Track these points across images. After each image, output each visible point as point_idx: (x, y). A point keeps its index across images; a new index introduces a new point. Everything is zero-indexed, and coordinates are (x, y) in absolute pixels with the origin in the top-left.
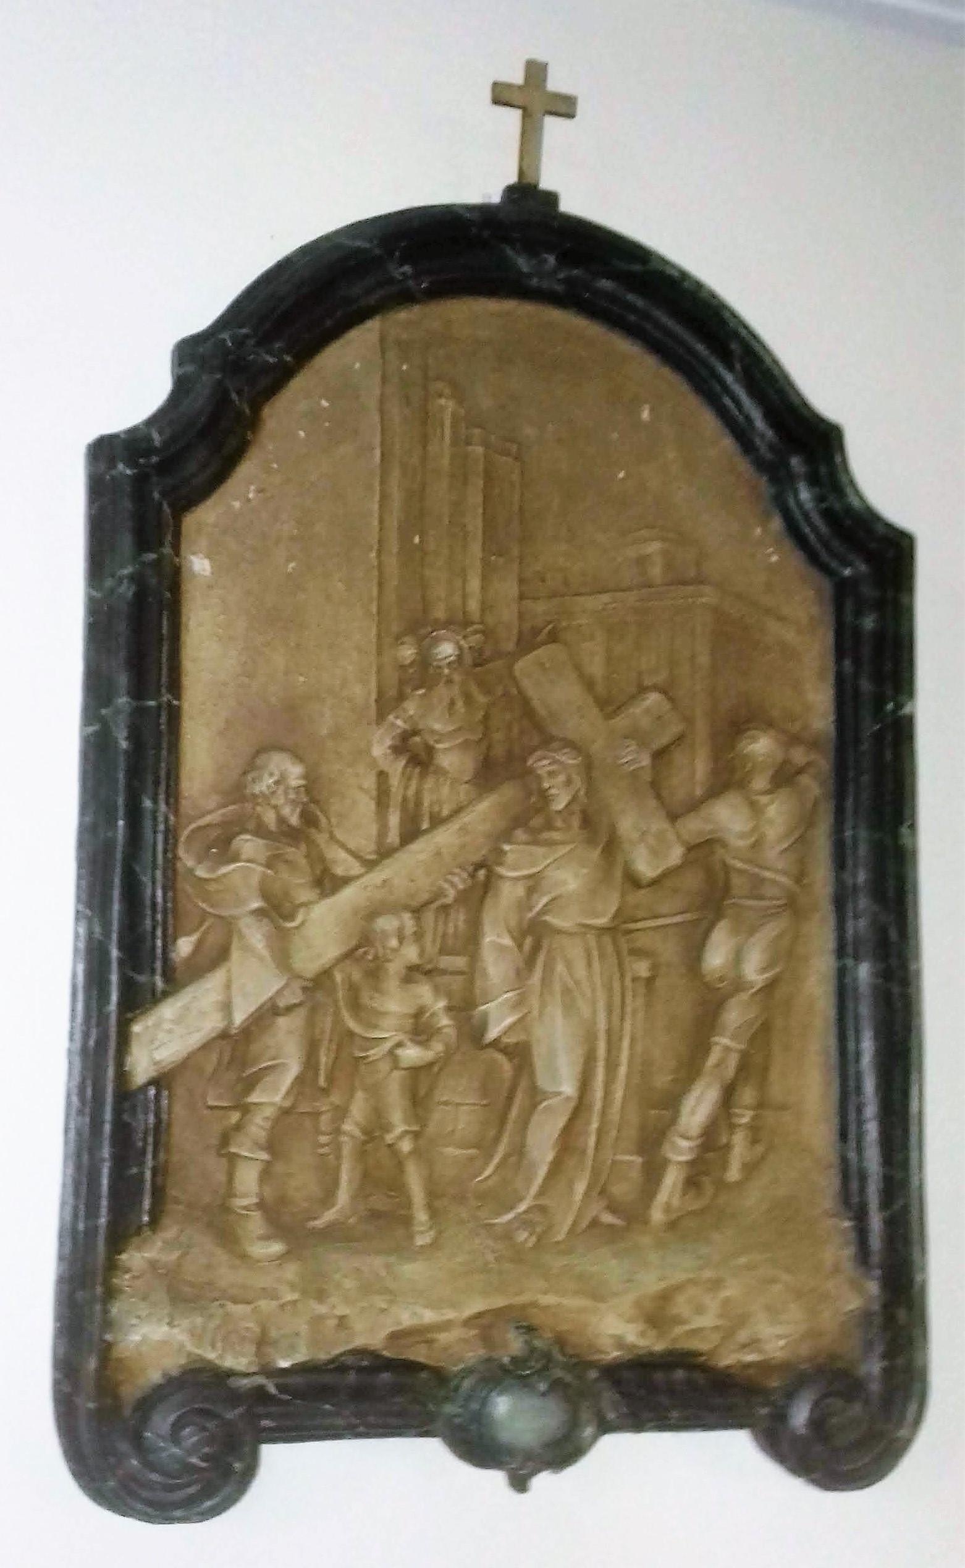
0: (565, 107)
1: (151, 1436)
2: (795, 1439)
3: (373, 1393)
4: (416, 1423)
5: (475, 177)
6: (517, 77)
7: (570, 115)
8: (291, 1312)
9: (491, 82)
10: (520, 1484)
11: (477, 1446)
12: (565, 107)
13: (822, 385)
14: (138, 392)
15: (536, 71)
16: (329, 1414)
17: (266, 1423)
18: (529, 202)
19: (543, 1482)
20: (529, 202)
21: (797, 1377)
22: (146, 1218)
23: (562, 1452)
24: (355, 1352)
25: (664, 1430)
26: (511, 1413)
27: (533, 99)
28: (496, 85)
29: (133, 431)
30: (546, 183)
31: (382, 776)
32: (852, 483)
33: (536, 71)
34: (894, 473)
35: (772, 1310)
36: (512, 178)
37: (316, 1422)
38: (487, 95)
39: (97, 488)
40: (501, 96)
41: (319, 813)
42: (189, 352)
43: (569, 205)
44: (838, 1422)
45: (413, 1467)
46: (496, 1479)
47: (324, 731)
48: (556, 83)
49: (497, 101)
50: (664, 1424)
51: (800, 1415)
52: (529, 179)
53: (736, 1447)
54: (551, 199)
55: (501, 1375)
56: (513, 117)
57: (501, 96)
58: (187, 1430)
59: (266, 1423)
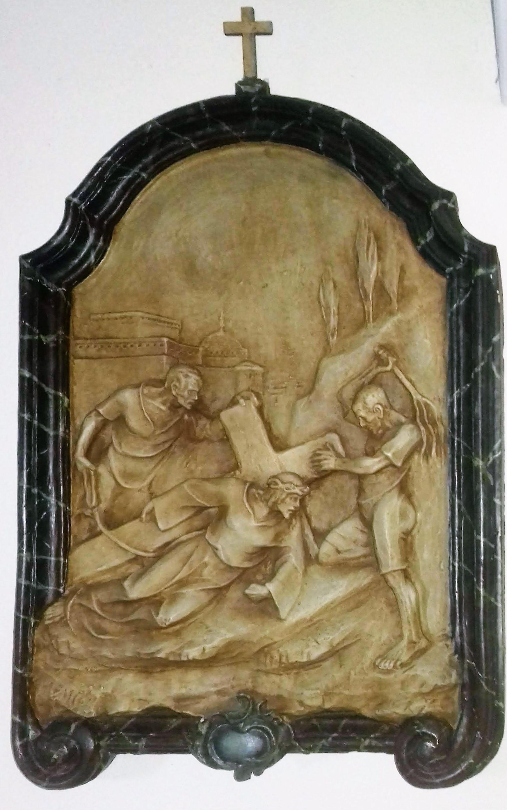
0: (267, 30)
1: (60, 745)
3: (159, 731)
5: (222, 83)
6: (237, 17)
7: (271, 34)
11: (214, 754)
13: (436, 171)
14: (43, 224)
15: (248, 13)
24: (118, 713)
26: (251, 743)
27: (249, 29)
30: (261, 76)
32: (49, 243)
33: (248, 13)
34: (479, 220)
35: (424, 683)
36: (240, 77)
37: (374, 723)
39: (22, 268)
40: (231, 30)
44: (439, 745)
45: (181, 768)
46: (228, 775)
54: (265, 86)
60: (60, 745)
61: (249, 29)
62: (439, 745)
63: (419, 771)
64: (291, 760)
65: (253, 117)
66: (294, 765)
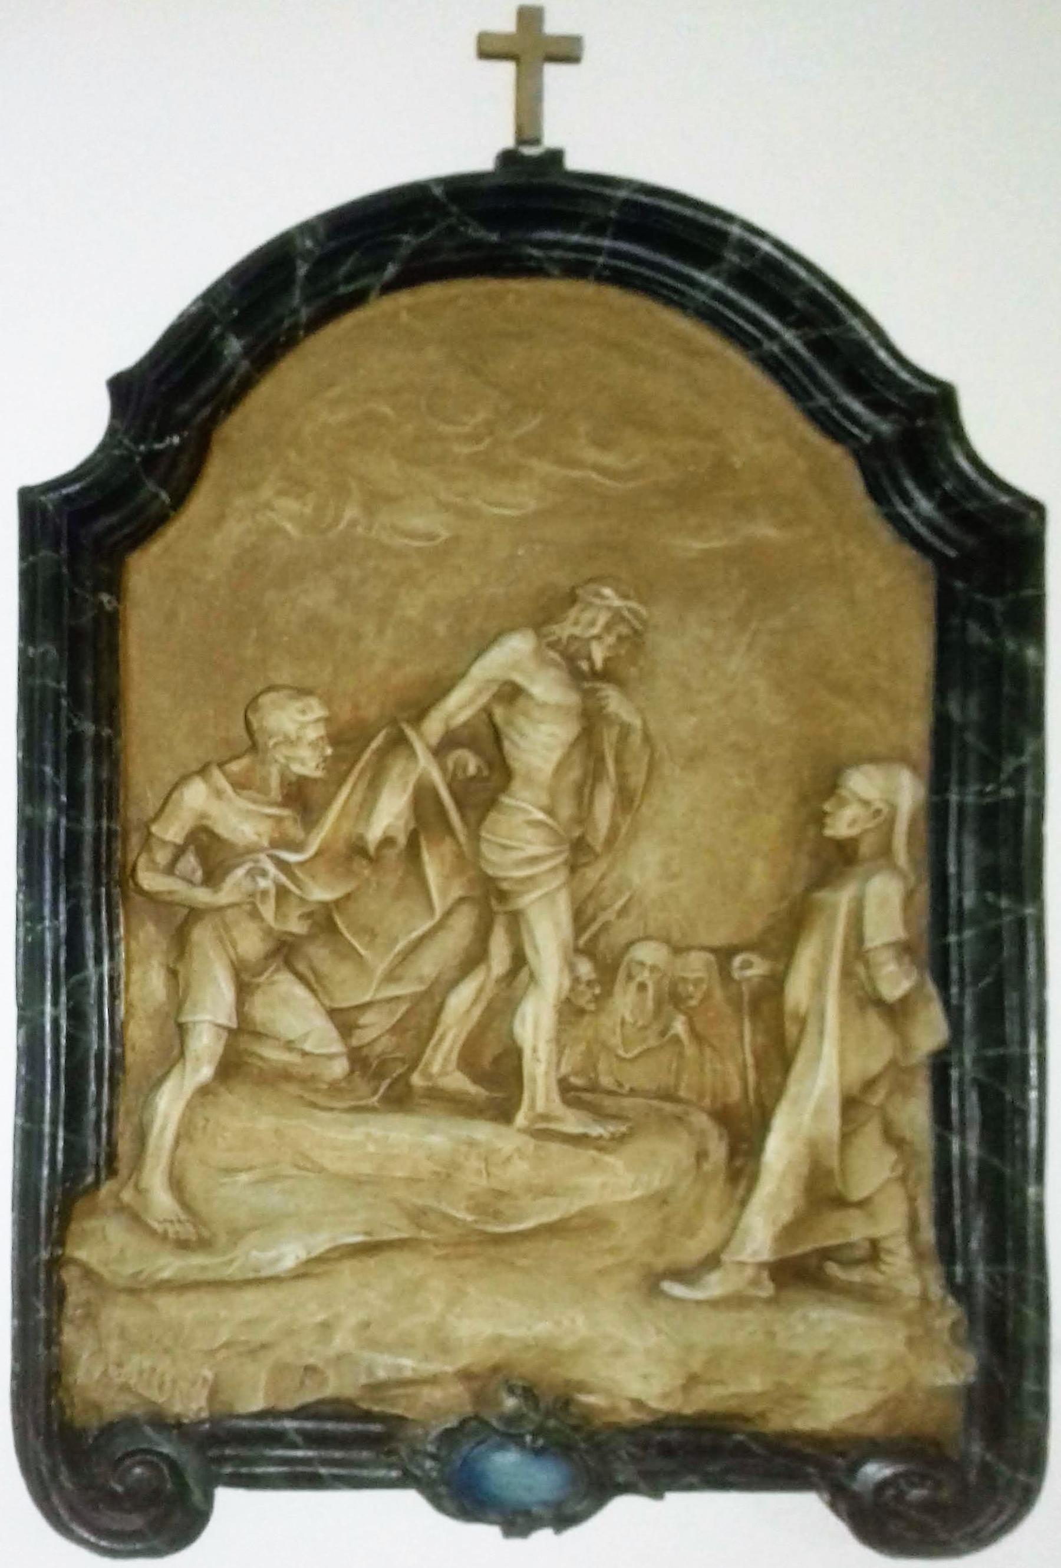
0: (567, 52)
1: (122, 1473)
3: (342, 1441)
5: (465, 139)
9: (476, 31)
11: (465, 1496)
12: (567, 52)
14: (72, 432)
15: (530, 18)
16: (57, 799)
22: (64, 702)
26: (509, 1468)
27: (530, 49)
30: (551, 139)
31: (712, 1261)
33: (530, 18)
36: (507, 140)
38: (472, 49)
40: (490, 49)
41: (122, 919)
42: (123, 388)
43: (574, 163)
47: (434, 1283)
48: (554, 25)
49: (485, 54)
54: (555, 157)
56: (507, 70)
61: (530, 49)
62: (930, 1482)
63: (872, 1520)
64: (626, 1511)
65: (521, 220)
66: (626, 1517)
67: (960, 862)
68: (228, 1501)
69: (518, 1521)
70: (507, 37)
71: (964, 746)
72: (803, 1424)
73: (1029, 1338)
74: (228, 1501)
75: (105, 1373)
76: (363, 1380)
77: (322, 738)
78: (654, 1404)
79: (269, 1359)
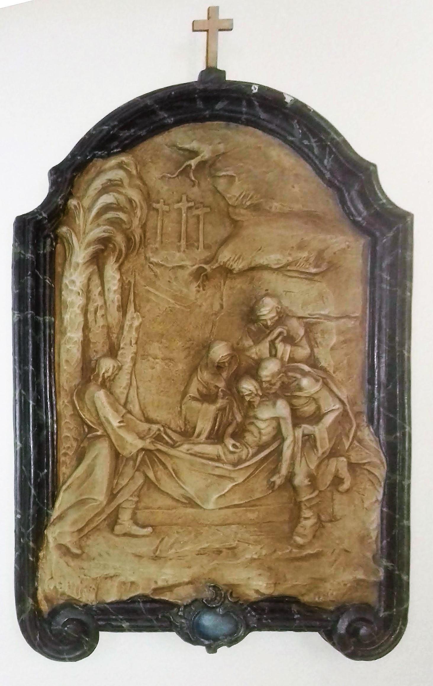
1: (59, 629)
2: (341, 637)
3: (145, 613)
4: (167, 626)
5: (184, 71)
8: (125, 568)
10: (211, 649)
11: (194, 635)
13: (363, 144)
14: (33, 194)
17: (100, 623)
18: (212, 74)
19: (223, 650)
20: (212, 74)
21: (341, 610)
23: (233, 639)
25: (286, 630)
28: (217, 8)
29: (32, 213)
30: (220, 67)
33: (212, 12)
34: (399, 187)
36: (203, 68)
40: (196, 27)
45: (164, 646)
46: (201, 650)
48: (223, 15)
50: (270, 628)
51: (342, 626)
52: (211, 64)
53: (315, 638)
55: (206, 606)
57: (196, 27)
58: (322, 137)
59: (100, 623)
60: (59, 629)
61: (212, 26)
64: (254, 637)
67: (379, 357)
68: (103, 635)
69: (213, 643)
70: (204, 21)
71: (381, 289)
72: (281, 141)
73: (405, 554)
74: (103, 635)
75: (55, 587)
76: (153, 586)
77: (115, 237)
78: (263, 591)
79: (117, 580)
